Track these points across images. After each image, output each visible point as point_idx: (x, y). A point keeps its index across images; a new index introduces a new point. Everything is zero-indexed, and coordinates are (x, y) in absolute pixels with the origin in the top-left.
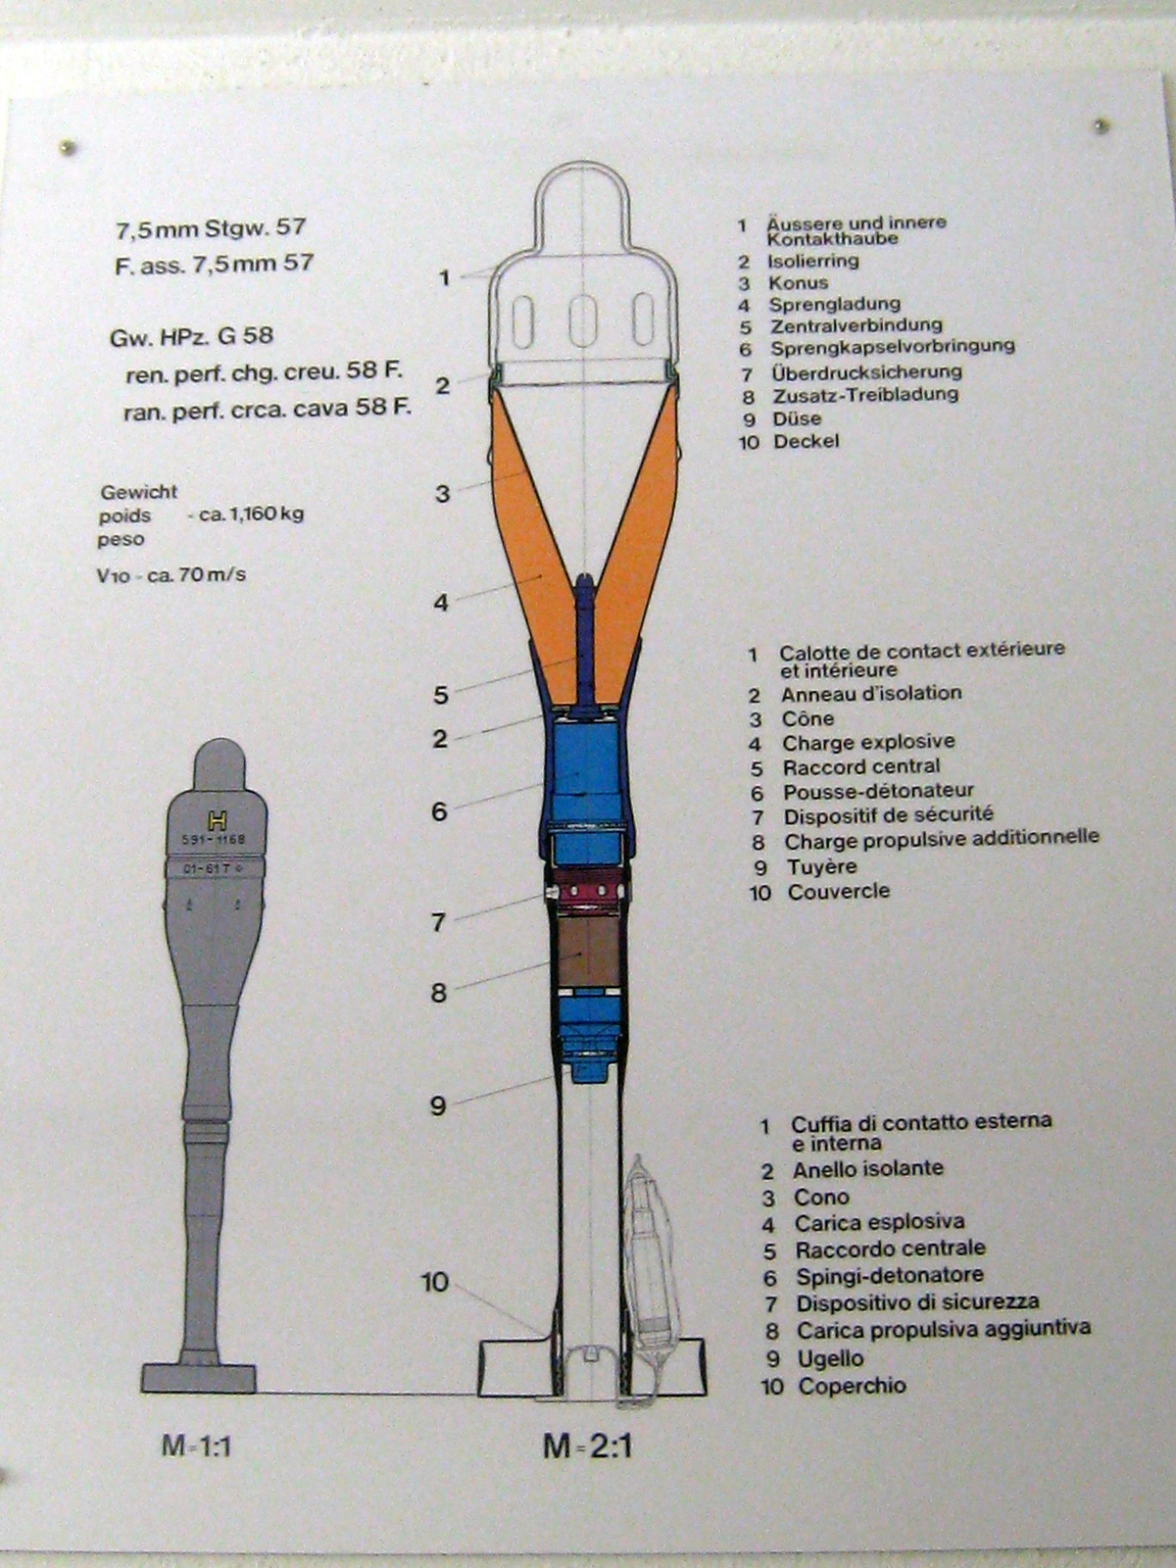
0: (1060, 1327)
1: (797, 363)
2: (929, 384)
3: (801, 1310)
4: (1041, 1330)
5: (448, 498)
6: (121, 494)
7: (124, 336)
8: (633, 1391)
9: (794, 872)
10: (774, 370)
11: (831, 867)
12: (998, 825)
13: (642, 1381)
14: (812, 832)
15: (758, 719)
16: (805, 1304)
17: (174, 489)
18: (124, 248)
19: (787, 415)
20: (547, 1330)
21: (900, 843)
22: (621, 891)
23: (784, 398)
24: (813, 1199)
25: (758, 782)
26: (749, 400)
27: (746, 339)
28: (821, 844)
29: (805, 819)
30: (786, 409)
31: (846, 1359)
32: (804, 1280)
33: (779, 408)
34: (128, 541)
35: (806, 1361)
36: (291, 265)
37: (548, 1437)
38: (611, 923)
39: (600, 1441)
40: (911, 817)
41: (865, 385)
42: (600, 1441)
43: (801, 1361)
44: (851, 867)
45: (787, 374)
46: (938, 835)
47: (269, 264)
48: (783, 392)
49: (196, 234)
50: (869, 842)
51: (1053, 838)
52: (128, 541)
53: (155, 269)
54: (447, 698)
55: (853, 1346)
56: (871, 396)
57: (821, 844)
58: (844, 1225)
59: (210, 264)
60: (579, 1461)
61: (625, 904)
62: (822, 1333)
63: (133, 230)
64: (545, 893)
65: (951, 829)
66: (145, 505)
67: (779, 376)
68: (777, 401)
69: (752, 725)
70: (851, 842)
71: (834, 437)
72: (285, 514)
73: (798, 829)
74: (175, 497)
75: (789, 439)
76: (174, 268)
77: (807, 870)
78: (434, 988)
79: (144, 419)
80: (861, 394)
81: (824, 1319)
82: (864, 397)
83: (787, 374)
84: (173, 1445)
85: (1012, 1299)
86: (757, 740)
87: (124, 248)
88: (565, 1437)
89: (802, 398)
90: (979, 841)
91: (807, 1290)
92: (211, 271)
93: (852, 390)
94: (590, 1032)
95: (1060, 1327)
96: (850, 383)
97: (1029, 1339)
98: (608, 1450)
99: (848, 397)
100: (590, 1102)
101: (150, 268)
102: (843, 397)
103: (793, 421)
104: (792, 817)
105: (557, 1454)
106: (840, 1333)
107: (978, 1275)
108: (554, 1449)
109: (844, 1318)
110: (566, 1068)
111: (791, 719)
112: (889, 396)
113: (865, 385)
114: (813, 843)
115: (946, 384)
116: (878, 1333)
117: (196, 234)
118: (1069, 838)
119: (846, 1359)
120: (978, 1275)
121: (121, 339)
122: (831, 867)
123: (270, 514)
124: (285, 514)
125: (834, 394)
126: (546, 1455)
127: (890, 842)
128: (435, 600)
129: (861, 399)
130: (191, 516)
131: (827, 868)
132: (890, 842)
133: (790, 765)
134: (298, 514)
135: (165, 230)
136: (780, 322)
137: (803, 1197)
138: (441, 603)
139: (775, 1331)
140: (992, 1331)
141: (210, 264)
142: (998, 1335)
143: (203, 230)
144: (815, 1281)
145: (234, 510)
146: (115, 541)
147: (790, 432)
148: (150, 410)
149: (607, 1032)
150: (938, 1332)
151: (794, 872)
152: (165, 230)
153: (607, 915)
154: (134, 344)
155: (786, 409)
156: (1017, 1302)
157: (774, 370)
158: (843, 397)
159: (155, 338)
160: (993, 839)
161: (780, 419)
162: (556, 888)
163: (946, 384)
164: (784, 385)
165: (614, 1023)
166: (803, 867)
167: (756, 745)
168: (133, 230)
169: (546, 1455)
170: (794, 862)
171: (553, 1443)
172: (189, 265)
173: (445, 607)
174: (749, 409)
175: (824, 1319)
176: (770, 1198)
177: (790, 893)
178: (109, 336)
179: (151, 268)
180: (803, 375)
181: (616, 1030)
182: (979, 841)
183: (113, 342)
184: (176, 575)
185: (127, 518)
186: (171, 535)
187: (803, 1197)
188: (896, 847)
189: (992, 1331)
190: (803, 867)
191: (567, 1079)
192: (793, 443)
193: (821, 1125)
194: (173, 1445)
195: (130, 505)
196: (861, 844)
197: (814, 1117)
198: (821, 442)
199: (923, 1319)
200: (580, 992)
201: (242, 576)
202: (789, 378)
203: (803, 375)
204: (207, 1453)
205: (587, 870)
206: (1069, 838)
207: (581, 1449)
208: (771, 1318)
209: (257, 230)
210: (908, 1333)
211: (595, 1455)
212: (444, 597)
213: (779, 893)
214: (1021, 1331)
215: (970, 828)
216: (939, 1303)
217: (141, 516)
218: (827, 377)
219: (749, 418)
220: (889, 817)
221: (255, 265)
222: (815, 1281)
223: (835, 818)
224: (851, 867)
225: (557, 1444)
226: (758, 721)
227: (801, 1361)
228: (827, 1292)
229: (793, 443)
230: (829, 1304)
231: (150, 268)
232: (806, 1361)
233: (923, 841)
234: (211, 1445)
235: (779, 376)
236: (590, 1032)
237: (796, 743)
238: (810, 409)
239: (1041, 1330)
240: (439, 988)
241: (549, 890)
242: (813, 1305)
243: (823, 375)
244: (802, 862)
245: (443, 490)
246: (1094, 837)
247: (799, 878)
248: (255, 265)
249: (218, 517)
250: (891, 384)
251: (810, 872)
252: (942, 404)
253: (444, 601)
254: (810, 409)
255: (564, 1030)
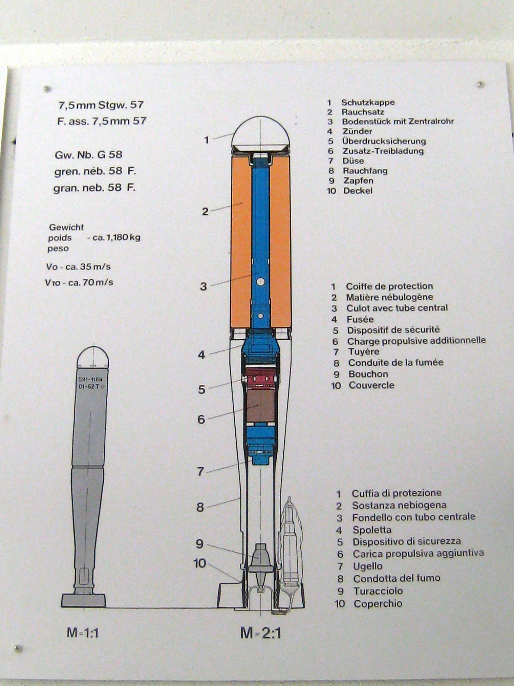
0: (469, 553)
1: (353, 137)
2: (411, 147)
3: (354, 545)
4: (462, 554)
5: (206, 288)
6: (58, 228)
7: (61, 154)
8: (280, 606)
9: (351, 354)
10: (343, 139)
11: (367, 352)
12: (442, 335)
13: (284, 601)
14: (360, 337)
15: (335, 308)
16: (356, 542)
17: (82, 226)
18: (62, 113)
19: (349, 159)
20: (241, 579)
21: (398, 342)
22: (275, 379)
23: (347, 152)
24: (362, 580)
25: (336, 336)
26: (331, 172)
27: (330, 146)
28: (364, 343)
29: (356, 331)
30: (348, 156)
31: (374, 566)
32: (356, 507)
33: (345, 156)
34: (61, 249)
35: (357, 567)
36: (134, 106)
37: (243, 629)
38: (271, 393)
39: (266, 630)
40: (403, 331)
41: (383, 147)
42: (266, 630)
43: (354, 567)
44: (377, 352)
45: (349, 141)
46: (415, 339)
47: (126, 121)
48: (347, 149)
49: (95, 107)
50: (385, 342)
51: (466, 341)
52: (61, 249)
53: (75, 122)
54: (204, 391)
55: (378, 561)
56: (385, 152)
57: (364, 343)
58: (375, 555)
59: (100, 121)
60: (257, 640)
61: (277, 385)
62: (364, 555)
63: (66, 105)
64: (241, 380)
65: (421, 336)
66: (68, 233)
67: (345, 141)
68: (345, 182)
69: (333, 311)
70: (376, 342)
71: (370, 189)
72: (131, 238)
73: (353, 336)
74: (82, 229)
75: (350, 189)
76: (84, 122)
77: (357, 353)
78: (198, 505)
79: (69, 191)
80: (381, 151)
81: (365, 549)
82: (383, 152)
83: (349, 141)
84: (72, 632)
85: (449, 540)
86: (330, 130)
87: (62, 113)
88: (251, 629)
89: (356, 152)
90: (433, 342)
91: (358, 536)
92: (100, 124)
93: (377, 149)
94: (261, 442)
95: (469, 553)
96: (376, 146)
97: (456, 558)
98: (270, 635)
99: (376, 152)
100: (261, 474)
101: (73, 122)
102: (373, 152)
103: (352, 162)
104: (351, 330)
105: (247, 637)
106: (372, 555)
107: (430, 297)
108: (245, 634)
109: (373, 548)
110: (250, 459)
111: (350, 308)
112: (393, 152)
113: (383, 147)
114: (360, 342)
115: (418, 147)
116: (389, 555)
117: (95, 107)
118: (473, 341)
119: (374, 566)
120: (430, 297)
121: (60, 155)
122: (367, 352)
123: (125, 237)
124: (131, 238)
125: (369, 151)
126: (242, 637)
127: (394, 342)
128: (198, 354)
129: (381, 153)
130: (89, 238)
131: (366, 352)
132: (394, 342)
133: (346, 169)
134: (138, 238)
135: (80, 105)
136: (348, 178)
137: (352, 363)
138: (201, 355)
139: (338, 363)
140: (440, 554)
141: (100, 121)
142: (442, 556)
143: (97, 105)
144: (361, 531)
145: (109, 236)
146: (55, 249)
147: (352, 186)
148: (72, 187)
149: (269, 442)
150: (410, 342)
151: (351, 354)
152: (80, 105)
153: (269, 389)
154: (65, 157)
155: (348, 156)
156: (451, 541)
157: (343, 139)
158: (373, 152)
159: (75, 155)
160: (440, 341)
161: (346, 161)
162: (246, 377)
163: (418, 147)
164: (347, 146)
165: (272, 438)
166: (355, 351)
167: (335, 320)
168: (66, 105)
169: (242, 637)
170: (357, 588)
171: (245, 632)
172: (91, 121)
173: (203, 357)
174: (331, 176)
175: (365, 549)
176: (340, 518)
177: (349, 362)
178: (55, 154)
179: (74, 122)
180: (356, 142)
181: (273, 441)
182: (433, 342)
183: (56, 156)
184: (81, 282)
185: (61, 238)
186: (80, 249)
187: (352, 363)
188: (401, 557)
189: (440, 554)
190: (355, 351)
191: (250, 464)
192: (352, 191)
193: (365, 494)
194: (72, 632)
195: (63, 233)
196: (381, 343)
197: (362, 490)
198: (365, 191)
199: (409, 549)
200: (257, 424)
201: (111, 283)
202: (350, 143)
203: (356, 142)
204: (87, 636)
205: (261, 363)
206: (473, 341)
207: (257, 634)
208: (331, 166)
209: (122, 106)
210: (403, 555)
211: (264, 637)
212: (203, 352)
213: (349, 604)
214: (453, 554)
215: (429, 336)
216: (416, 542)
217: (67, 238)
218: (366, 143)
219: (332, 180)
220: (394, 331)
221: (120, 122)
222: (361, 531)
223: (370, 331)
224: (377, 352)
225: (247, 633)
226: (335, 309)
227: (354, 567)
228: (366, 537)
229: (352, 191)
230: (361, 330)
231: (73, 122)
232: (357, 567)
233: (408, 342)
234: (89, 632)
235: (345, 141)
236: (261, 442)
237: (354, 341)
238: (358, 157)
239: (462, 554)
240: (200, 505)
241: (243, 378)
242: (360, 543)
243: (365, 142)
244: (361, 588)
245: (204, 285)
246: (483, 341)
247: (354, 356)
248: (120, 122)
249: (101, 238)
250: (394, 147)
251: (359, 354)
252: (417, 156)
253: (203, 354)
254: (358, 157)
255: (248, 441)
